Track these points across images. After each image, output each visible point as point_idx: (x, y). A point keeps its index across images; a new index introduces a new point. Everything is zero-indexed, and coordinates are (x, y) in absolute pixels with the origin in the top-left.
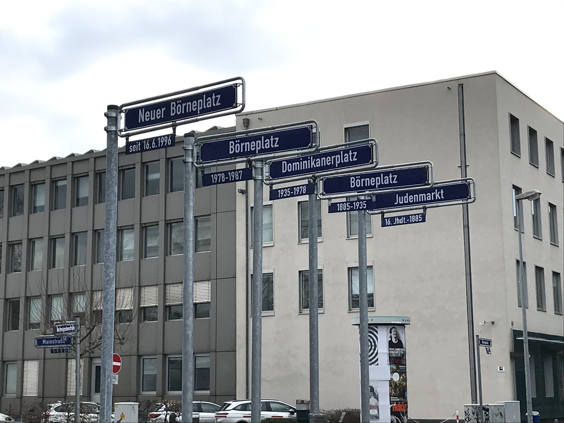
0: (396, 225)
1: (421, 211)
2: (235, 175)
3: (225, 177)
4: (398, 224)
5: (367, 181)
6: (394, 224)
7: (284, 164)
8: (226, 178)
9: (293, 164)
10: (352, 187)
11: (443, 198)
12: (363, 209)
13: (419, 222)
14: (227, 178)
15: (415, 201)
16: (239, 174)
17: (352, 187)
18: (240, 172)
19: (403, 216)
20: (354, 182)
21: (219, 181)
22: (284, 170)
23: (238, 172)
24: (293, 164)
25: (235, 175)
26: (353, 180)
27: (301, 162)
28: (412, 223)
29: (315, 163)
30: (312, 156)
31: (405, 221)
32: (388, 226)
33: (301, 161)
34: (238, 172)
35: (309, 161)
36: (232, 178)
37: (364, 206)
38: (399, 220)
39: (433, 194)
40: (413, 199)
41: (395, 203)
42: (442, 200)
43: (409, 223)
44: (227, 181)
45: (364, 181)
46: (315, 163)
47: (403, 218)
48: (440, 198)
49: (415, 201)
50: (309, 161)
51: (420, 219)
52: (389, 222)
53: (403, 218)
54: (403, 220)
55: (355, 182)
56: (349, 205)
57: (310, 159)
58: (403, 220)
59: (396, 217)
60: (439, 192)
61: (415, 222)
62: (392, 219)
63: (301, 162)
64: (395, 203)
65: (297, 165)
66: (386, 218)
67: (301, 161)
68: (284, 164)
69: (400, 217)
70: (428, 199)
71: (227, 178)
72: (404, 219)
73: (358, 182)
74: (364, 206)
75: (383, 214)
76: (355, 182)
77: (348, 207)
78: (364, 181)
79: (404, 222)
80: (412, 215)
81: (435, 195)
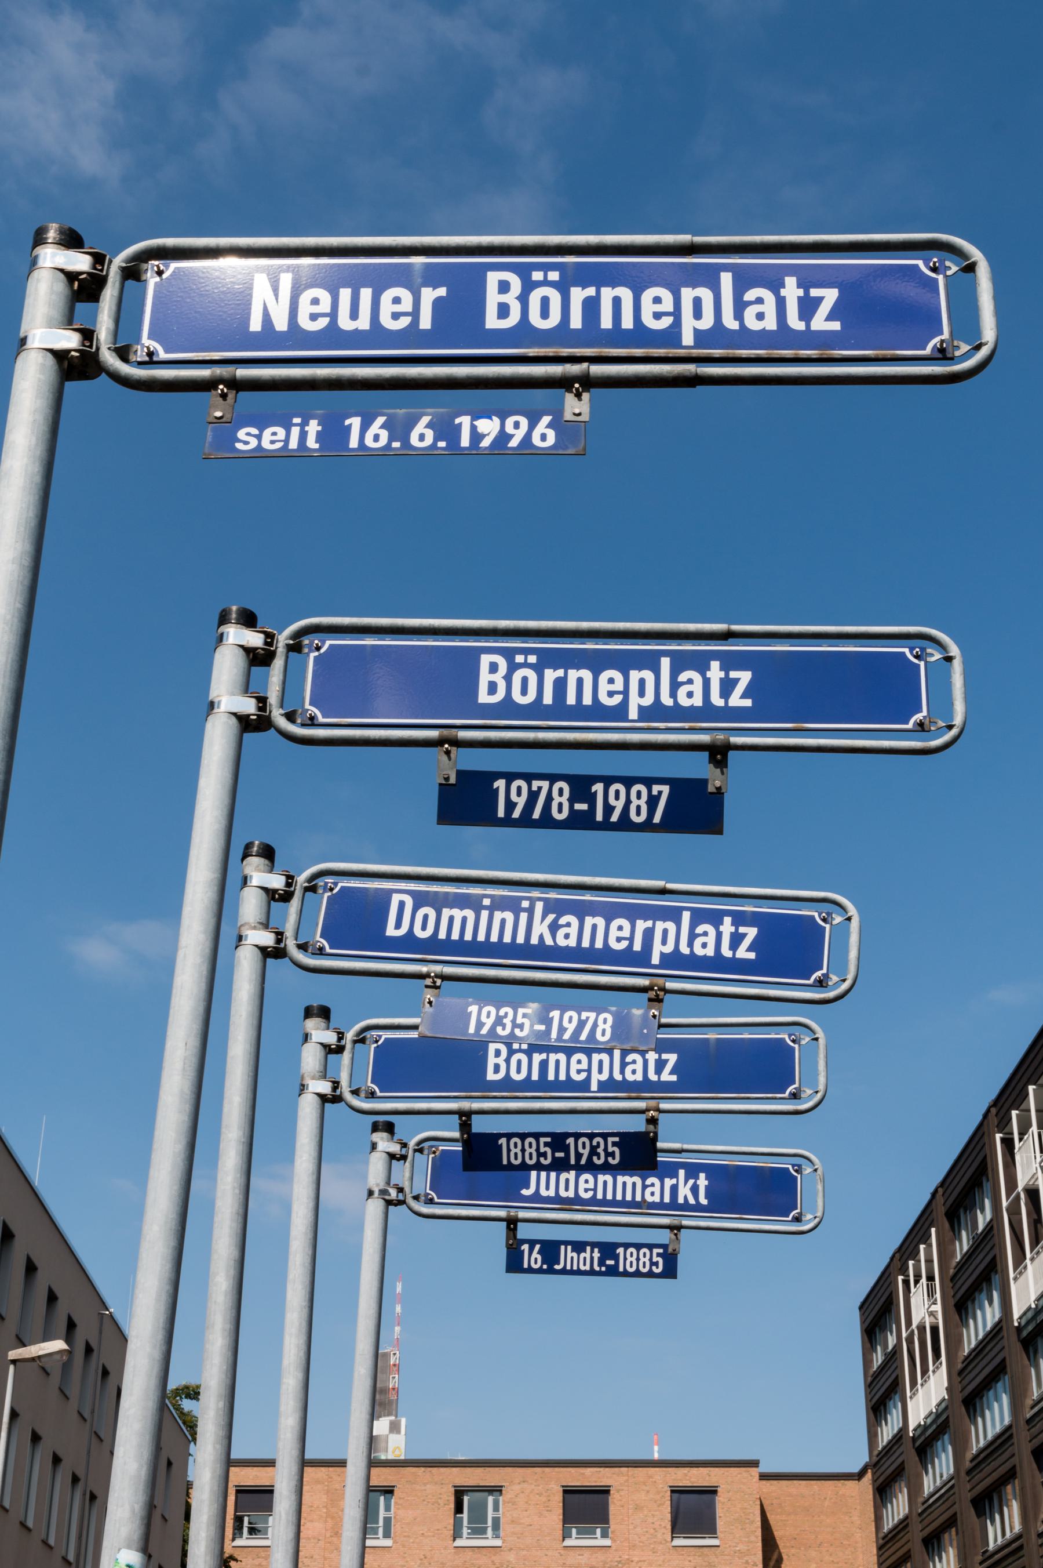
0: (564, 1271)
1: (664, 1237)
2: (628, 802)
3: (572, 801)
4: (572, 1272)
5: (557, 1062)
6: (557, 1267)
7: (402, 905)
8: (578, 806)
9: (446, 913)
10: (491, 1076)
11: (704, 1201)
12: (606, 1168)
13: (650, 1274)
14: (584, 807)
15: (600, 1196)
16: (653, 802)
17: (491, 1076)
18: (656, 789)
19: (594, 1245)
20: (501, 1061)
21: (536, 815)
22: (398, 925)
23: (650, 790)
24: (446, 913)
25: (628, 802)
26: (498, 1053)
27: (485, 914)
28: (626, 1274)
29: (554, 928)
30: (540, 899)
31: (600, 1264)
32: (530, 1270)
33: (486, 908)
34: (650, 790)
35: (523, 917)
36: (609, 809)
37: (613, 1155)
38: (575, 1255)
39: (669, 1182)
40: (595, 1190)
41: (524, 1192)
42: (698, 1207)
43: (613, 1271)
44: (579, 821)
45: (544, 1065)
46: (554, 928)
47: (592, 1252)
48: (692, 1201)
49: (600, 1196)
50: (523, 917)
51: (656, 1264)
52: (534, 1258)
53: (592, 1252)
54: (592, 1258)
55: (508, 1061)
56: (546, 1144)
57: (531, 911)
58: (592, 1258)
59: (566, 1243)
60: (691, 1182)
61: (638, 1274)
62: (550, 1250)
63: (485, 914)
64: (524, 1192)
65: (464, 920)
66: (524, 1241)
67: (486, 908)
68: (402, 905)
69: (579, 1247)
70: (649, 1198)
71: (584, 807)
72: (596, 1255)
73: (519, 1062)
74: (613, 1155)
75: (512, 1223)
76: (508, 1061)
77: (544, 1155)
78: (544, 1065)
79: (597, 1268)
80: (626, 1246)
81: (674, 1189)
